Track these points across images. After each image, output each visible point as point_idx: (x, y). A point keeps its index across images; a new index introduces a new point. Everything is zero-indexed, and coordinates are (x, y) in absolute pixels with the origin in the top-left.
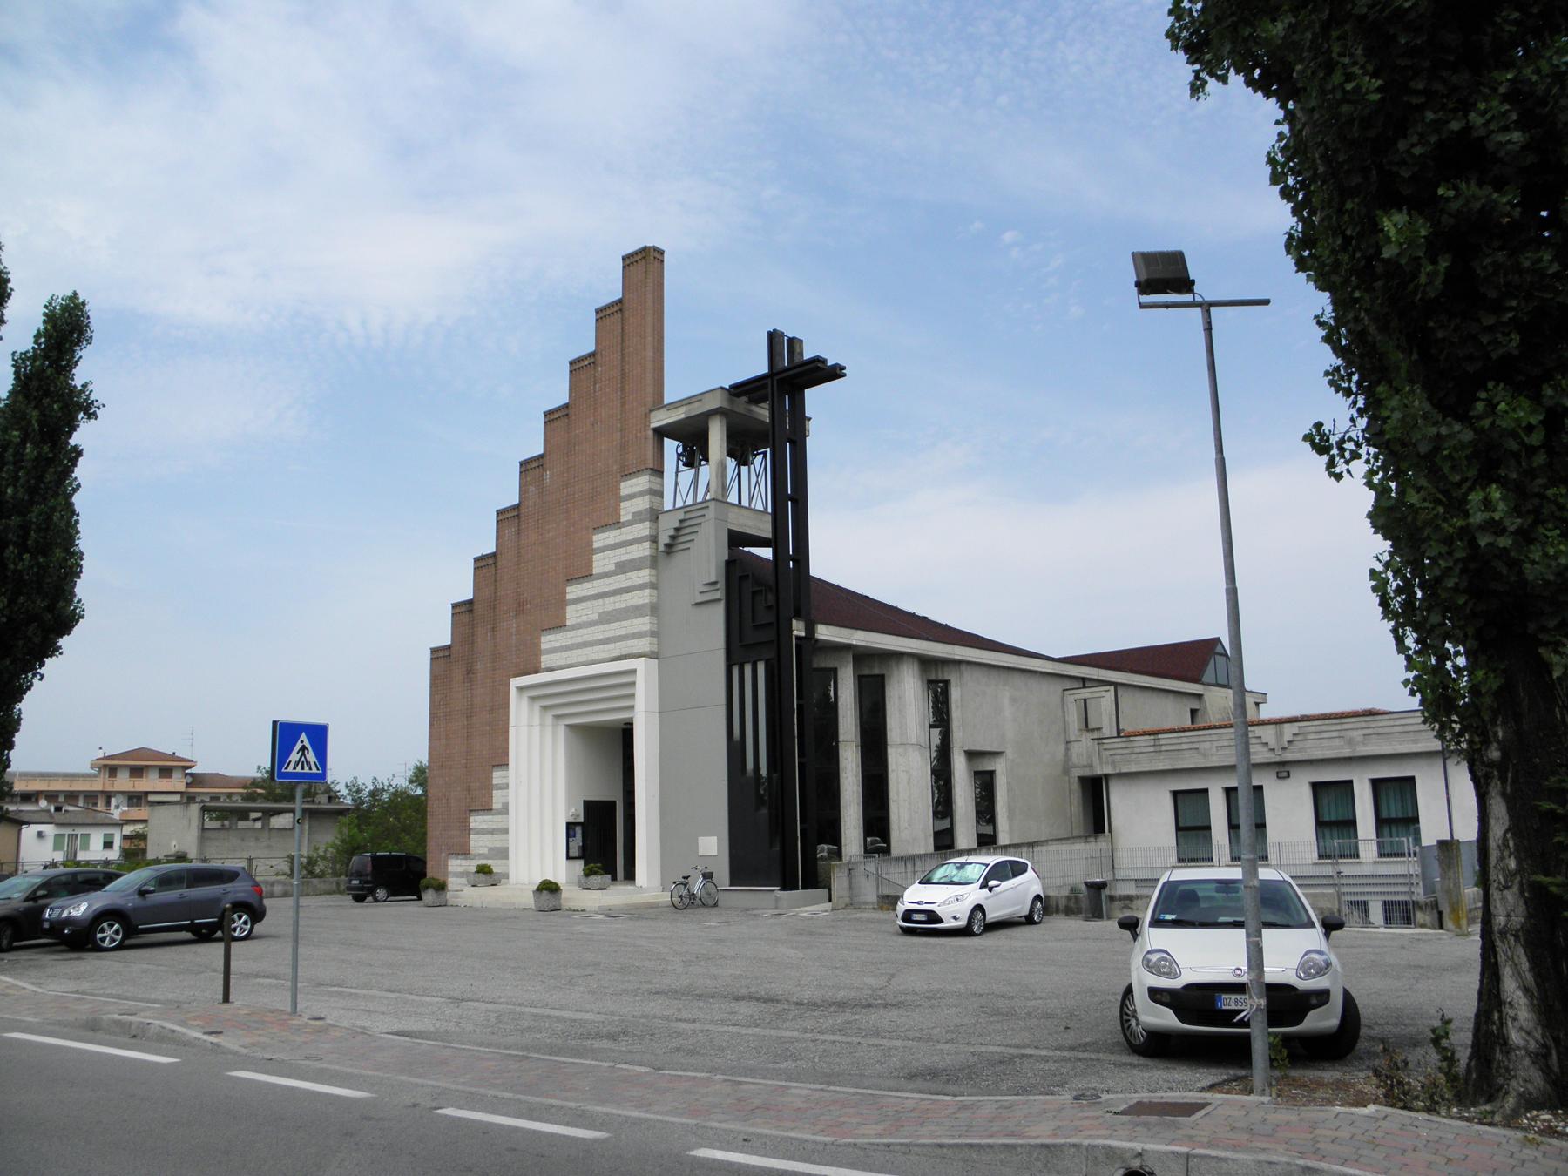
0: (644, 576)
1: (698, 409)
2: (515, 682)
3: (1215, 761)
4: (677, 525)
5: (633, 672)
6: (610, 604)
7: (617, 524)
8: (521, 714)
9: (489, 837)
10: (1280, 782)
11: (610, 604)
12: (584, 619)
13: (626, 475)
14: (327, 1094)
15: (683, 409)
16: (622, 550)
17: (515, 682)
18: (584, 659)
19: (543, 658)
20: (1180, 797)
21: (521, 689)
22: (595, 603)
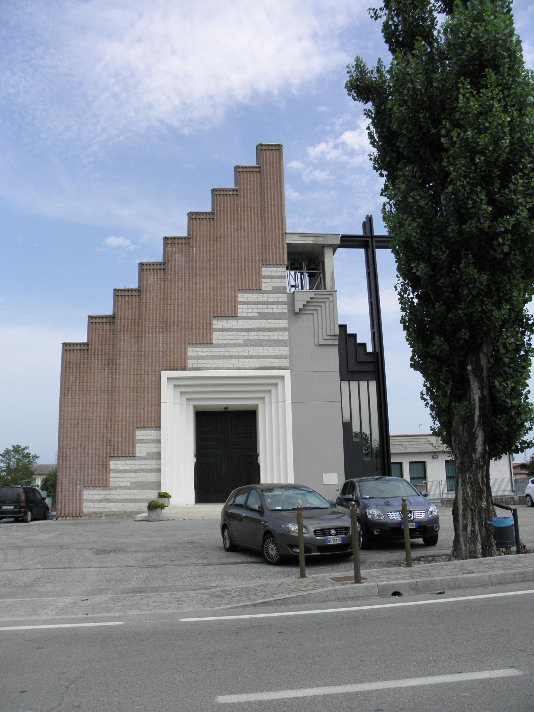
0: (284, 323)
1: (321, 241)
2: (165, 375)
3: (410, 450)
4: (309, 300)
5: (283, 378)
6: (253, 336)
7: (259, 290)
8: (169, 396)
9: (133, 475)
10: (433, 460)
11: (253, 336)
12: (231, 342)
13: (267, 264)
14: (505, 596)
15: (312, 239)
16: (265, 306)
17: (165, 375)
18: (231, 366)
19: (189, 362)
20: (399, 465)
21: (169, 379)
22: (241, 333)
